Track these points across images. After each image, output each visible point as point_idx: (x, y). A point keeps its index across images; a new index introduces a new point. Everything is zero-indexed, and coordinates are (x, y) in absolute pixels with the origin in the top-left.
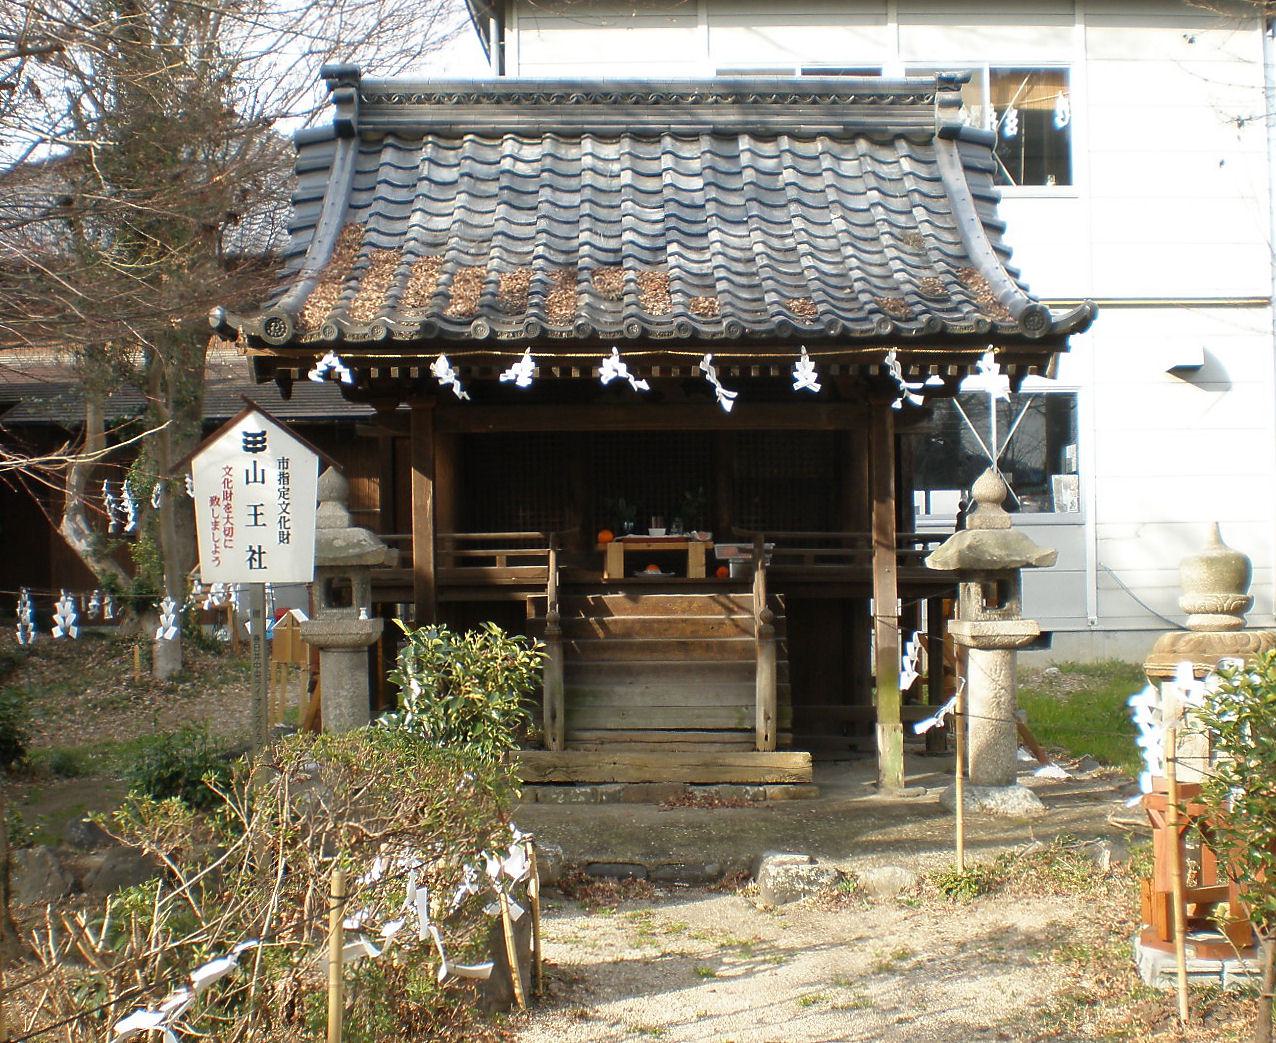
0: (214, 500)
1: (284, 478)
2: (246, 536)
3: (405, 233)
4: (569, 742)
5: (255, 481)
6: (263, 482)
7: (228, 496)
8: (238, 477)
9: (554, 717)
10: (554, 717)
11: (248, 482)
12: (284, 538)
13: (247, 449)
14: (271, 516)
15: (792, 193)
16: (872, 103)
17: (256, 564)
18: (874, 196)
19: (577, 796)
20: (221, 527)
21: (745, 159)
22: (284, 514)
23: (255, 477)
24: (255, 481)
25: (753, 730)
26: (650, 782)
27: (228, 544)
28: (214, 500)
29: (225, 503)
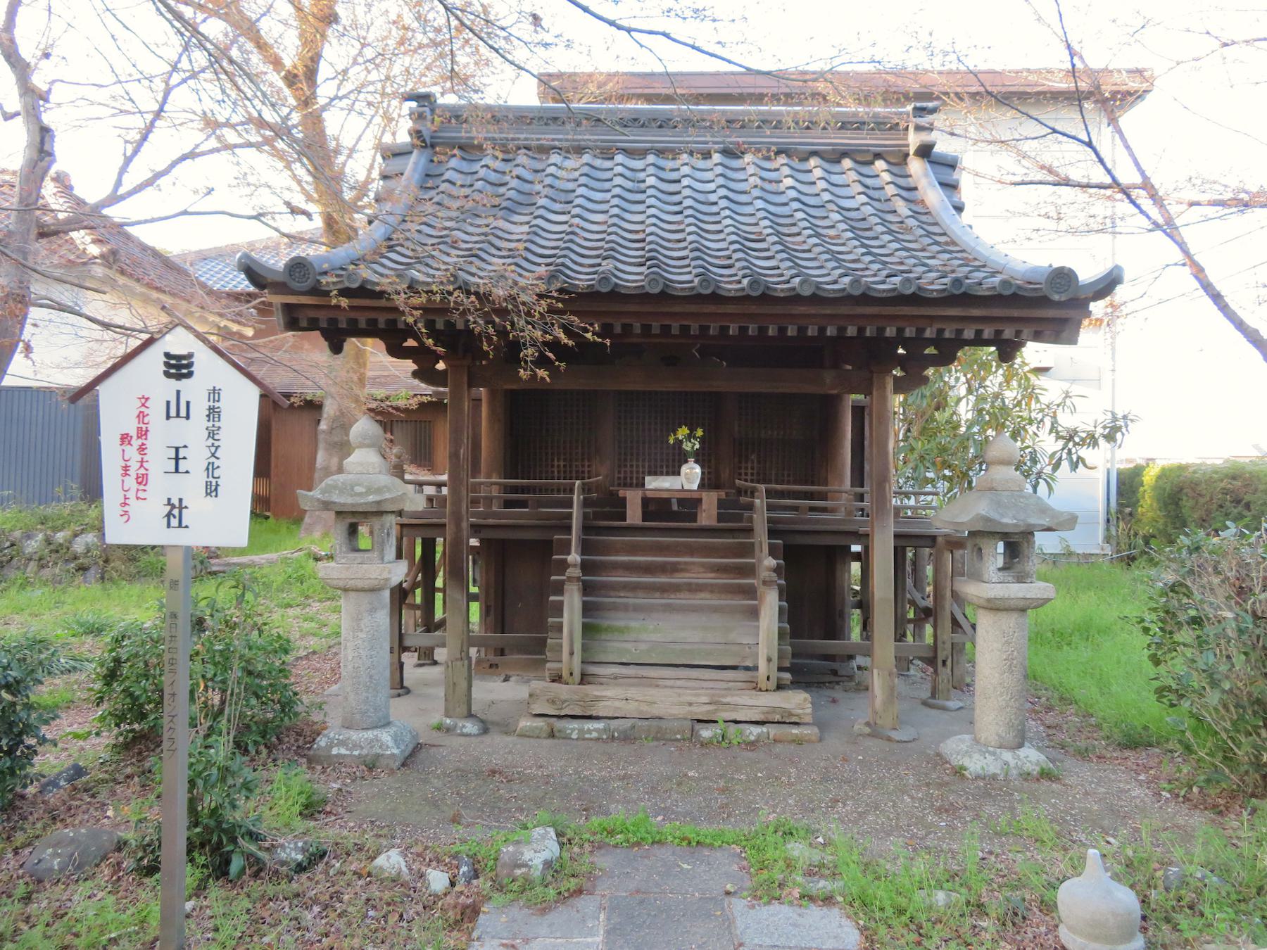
0: (125, 438)
1: (213, 413)
2: (162, 486)
3: (442, 175)
4: (585, 679)
5: (178, 415)
6: (188, 417)
7: (143, 433)
8: (156, 412)
9: (572, 654)
10: (572, 654)
11: (168, 417)
12: (212, 490)
13: (167, 374)
14: (196, 459)
15: (793, 194)
16: (855, 129)
17: (174, 522)
18: (863, 199)
19: (589, 731)
20: (132, 472)
21: (751, 169)
22: (213, 460)
23: (178, 410)
24: (178, 415)
25: (756, 668)
26: (661, 718)
27: (141, 494)
28: (125, 438)
29: (140, 442)
